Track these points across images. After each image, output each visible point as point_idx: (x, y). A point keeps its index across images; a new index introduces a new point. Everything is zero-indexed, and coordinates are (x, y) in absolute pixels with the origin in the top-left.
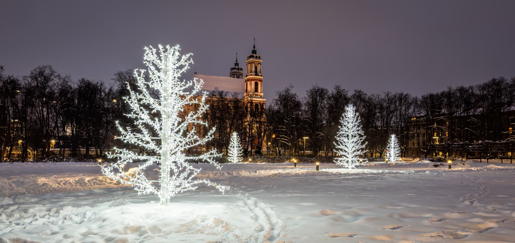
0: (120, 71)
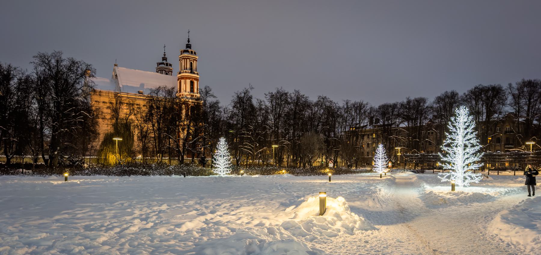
0: (42, 52)
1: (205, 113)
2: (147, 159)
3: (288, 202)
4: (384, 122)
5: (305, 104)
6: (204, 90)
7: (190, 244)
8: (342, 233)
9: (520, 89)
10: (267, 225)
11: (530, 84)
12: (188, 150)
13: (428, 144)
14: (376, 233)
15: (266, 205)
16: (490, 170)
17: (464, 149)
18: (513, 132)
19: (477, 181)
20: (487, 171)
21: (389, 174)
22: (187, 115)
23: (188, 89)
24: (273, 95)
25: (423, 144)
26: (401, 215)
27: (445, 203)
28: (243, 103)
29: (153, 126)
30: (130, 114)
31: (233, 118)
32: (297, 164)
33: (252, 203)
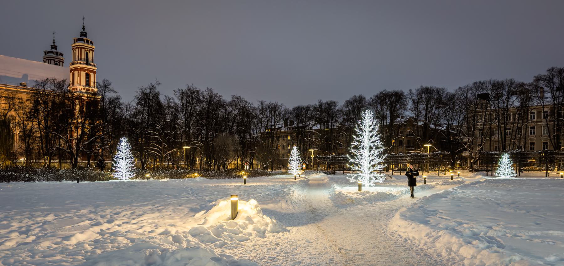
1: (103, 110)
2: (31, 163)
3: (199, 207)
4: (298, 124)
5: (218, 104)
6: (102, 84)
7: (80, 258)
8: (253, 236)
9: (419, 95)
10: (173, 233)
11: (427, 91)
12: (82, 152)
13: (338, 146)
14: (287, 235)
15: (174, 211)
16: (393, 170)
17: (370, 151)
18: (413, 135)
19: (381, 181)
20: (391, 172)
21: (303, 176)
22: (81, 111)
23: (83, 82)
24: (184, 93)
25: (334, 146)
26: (312, 216)
27: (353, 202)
28: (149, 99)
29: (39, 123)
30: (10, 109)
31: (137, 116)
32: (211, 166)
33: (158, 210)
